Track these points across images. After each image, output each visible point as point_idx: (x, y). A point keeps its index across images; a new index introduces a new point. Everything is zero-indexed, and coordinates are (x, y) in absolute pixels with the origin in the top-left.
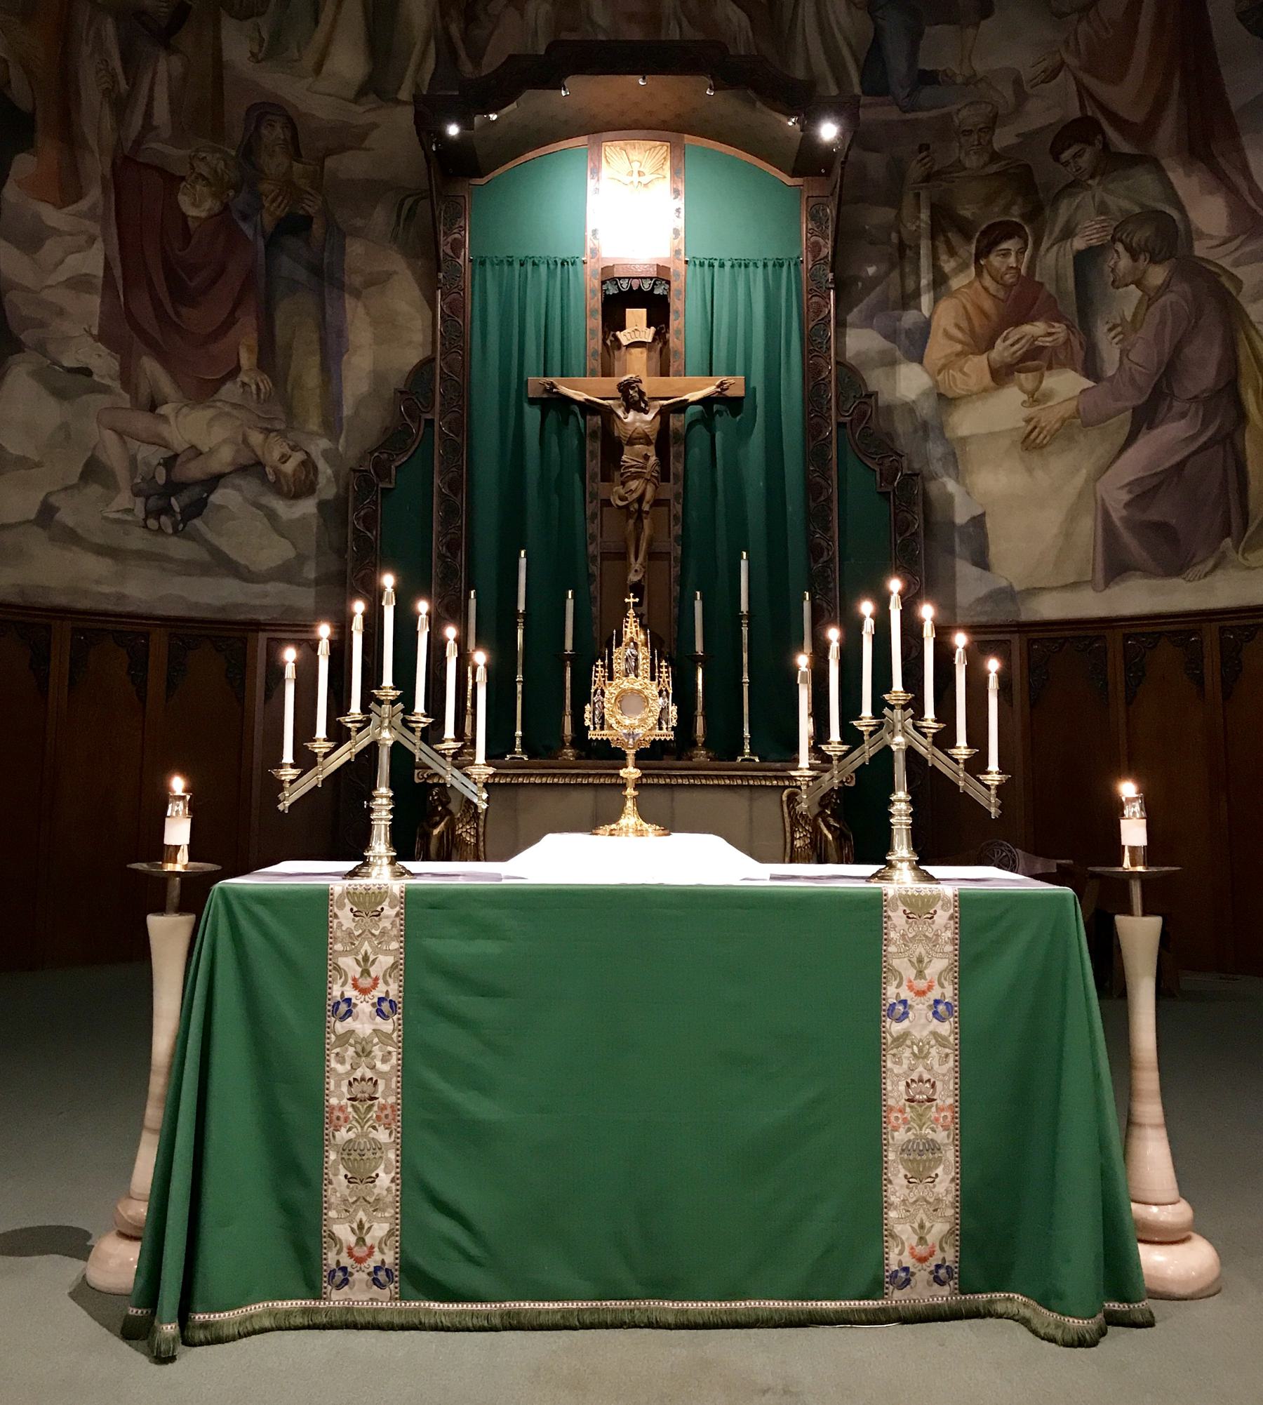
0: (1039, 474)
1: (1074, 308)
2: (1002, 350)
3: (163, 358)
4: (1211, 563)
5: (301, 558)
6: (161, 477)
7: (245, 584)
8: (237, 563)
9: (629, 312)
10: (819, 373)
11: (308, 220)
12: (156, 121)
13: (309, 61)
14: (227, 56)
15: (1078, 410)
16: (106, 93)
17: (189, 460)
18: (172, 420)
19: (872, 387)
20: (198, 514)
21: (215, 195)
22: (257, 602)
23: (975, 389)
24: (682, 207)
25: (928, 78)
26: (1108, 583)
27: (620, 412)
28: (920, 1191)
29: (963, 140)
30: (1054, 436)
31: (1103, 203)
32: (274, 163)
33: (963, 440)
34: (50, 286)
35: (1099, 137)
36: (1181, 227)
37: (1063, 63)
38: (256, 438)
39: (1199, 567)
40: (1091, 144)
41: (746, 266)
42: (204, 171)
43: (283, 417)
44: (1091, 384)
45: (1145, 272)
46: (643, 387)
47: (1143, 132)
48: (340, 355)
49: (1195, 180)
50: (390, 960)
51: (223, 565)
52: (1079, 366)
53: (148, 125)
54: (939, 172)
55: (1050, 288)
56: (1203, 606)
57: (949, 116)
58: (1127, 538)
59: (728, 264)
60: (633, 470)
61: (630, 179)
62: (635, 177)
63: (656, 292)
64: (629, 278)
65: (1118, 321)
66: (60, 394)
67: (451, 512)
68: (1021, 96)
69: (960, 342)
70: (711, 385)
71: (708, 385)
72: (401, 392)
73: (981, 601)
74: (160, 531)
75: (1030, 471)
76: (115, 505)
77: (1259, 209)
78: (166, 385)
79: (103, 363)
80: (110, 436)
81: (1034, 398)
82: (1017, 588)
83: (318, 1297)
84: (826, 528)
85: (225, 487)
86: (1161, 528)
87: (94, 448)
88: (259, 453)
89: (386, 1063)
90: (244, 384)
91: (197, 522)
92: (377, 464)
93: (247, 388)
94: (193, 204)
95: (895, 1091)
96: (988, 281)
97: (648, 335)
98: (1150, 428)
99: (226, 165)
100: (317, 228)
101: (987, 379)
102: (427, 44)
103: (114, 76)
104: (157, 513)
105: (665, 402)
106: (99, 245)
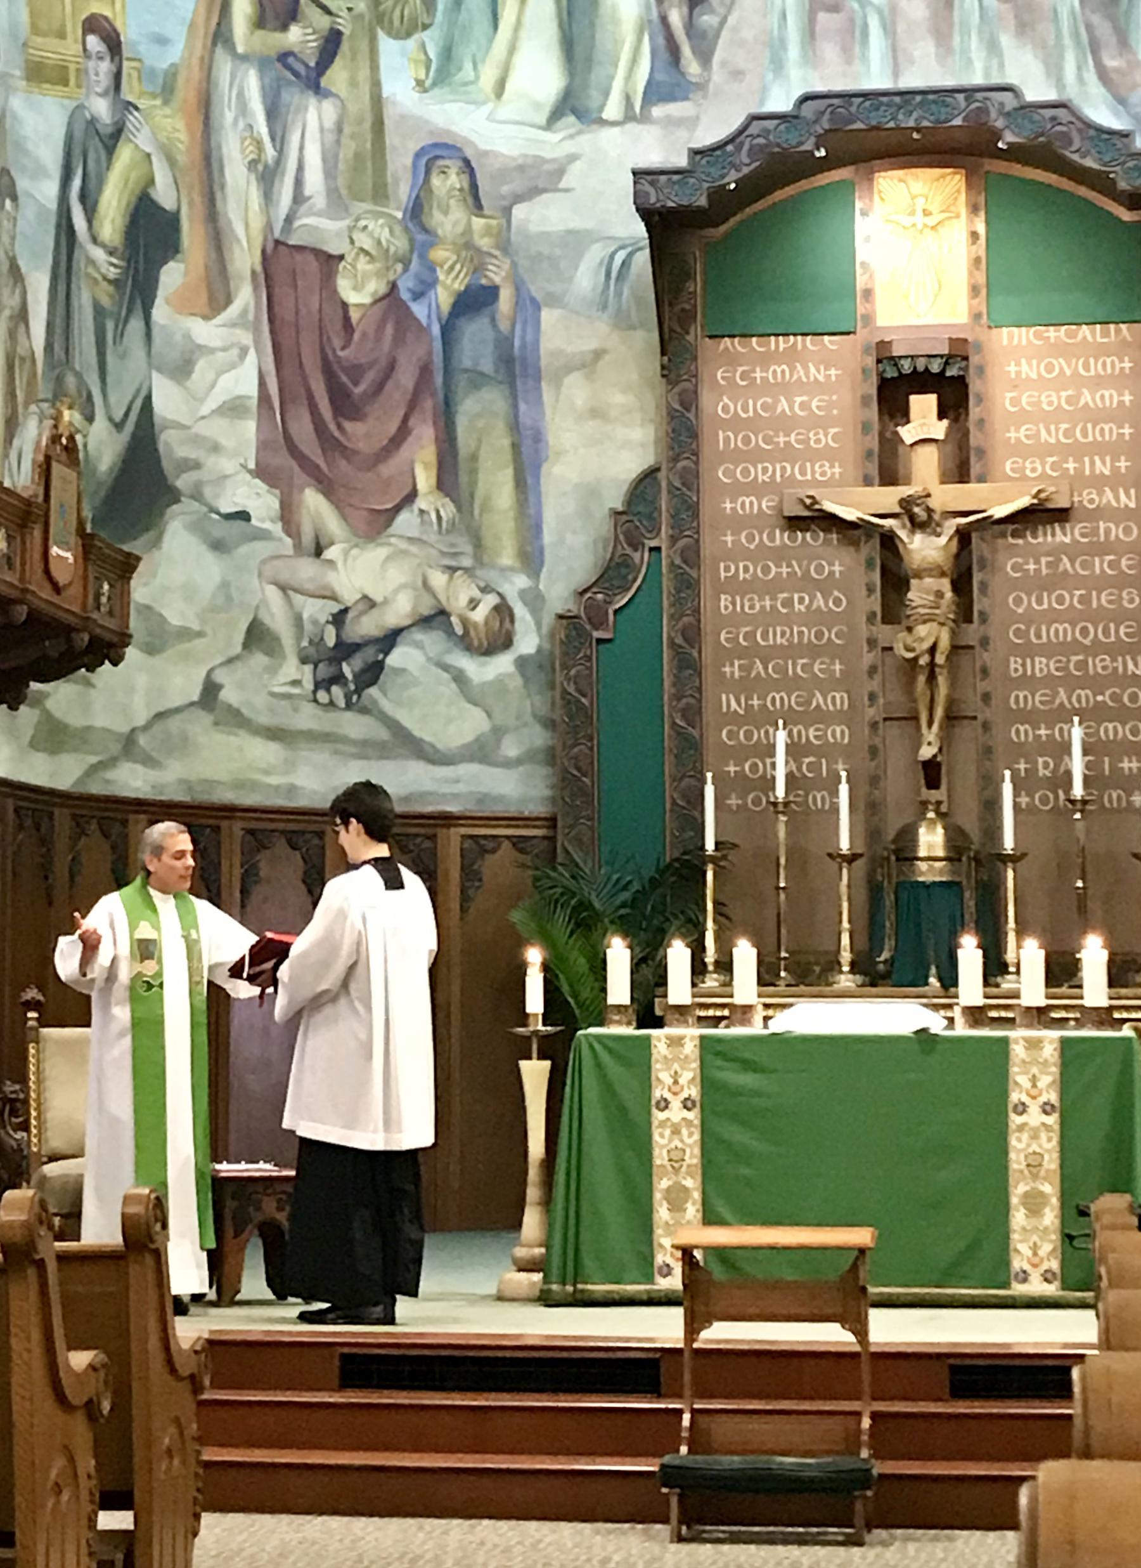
3: (327, 488)
5: (498, 732)
6: (331, 641)
7: (430, 767)
8: (421, 740)
11: (492, 292)
13: (488, 75)
14: (386, 91)
16: (252, 164)
18: (340, 565)
20: (373, 682)
21: (378, 274)
27: (903, 534)
28: (1034, 1221)
34: (203, 418)
38: (438, 579)
42: (368, 244)
43: (469, 549)
46: (933, 503)
48: (538, 467)
50: (690, 1075)
53: (299, 197)
60: (922, 611)
62: (919, 219)
63: (948, 374)
64: (912, 357)
66: (218, 546)
70: (1022, 495)
76: (282, 679)
78: (332, 523)
80: (272, 592)
83: (653, 1283)
87: (257, 607)
88: (442, 598)
89: (692, 1139)
90: (422, 512)
91: (373, 691)
92: (591, 606)
93: (426, 517)
94: (355, 288)
95: (1017, 1161)
97: (939, 429)
99: (391, 231)
102: (640, 40)
103: (259, 144)
106: (252, 358)
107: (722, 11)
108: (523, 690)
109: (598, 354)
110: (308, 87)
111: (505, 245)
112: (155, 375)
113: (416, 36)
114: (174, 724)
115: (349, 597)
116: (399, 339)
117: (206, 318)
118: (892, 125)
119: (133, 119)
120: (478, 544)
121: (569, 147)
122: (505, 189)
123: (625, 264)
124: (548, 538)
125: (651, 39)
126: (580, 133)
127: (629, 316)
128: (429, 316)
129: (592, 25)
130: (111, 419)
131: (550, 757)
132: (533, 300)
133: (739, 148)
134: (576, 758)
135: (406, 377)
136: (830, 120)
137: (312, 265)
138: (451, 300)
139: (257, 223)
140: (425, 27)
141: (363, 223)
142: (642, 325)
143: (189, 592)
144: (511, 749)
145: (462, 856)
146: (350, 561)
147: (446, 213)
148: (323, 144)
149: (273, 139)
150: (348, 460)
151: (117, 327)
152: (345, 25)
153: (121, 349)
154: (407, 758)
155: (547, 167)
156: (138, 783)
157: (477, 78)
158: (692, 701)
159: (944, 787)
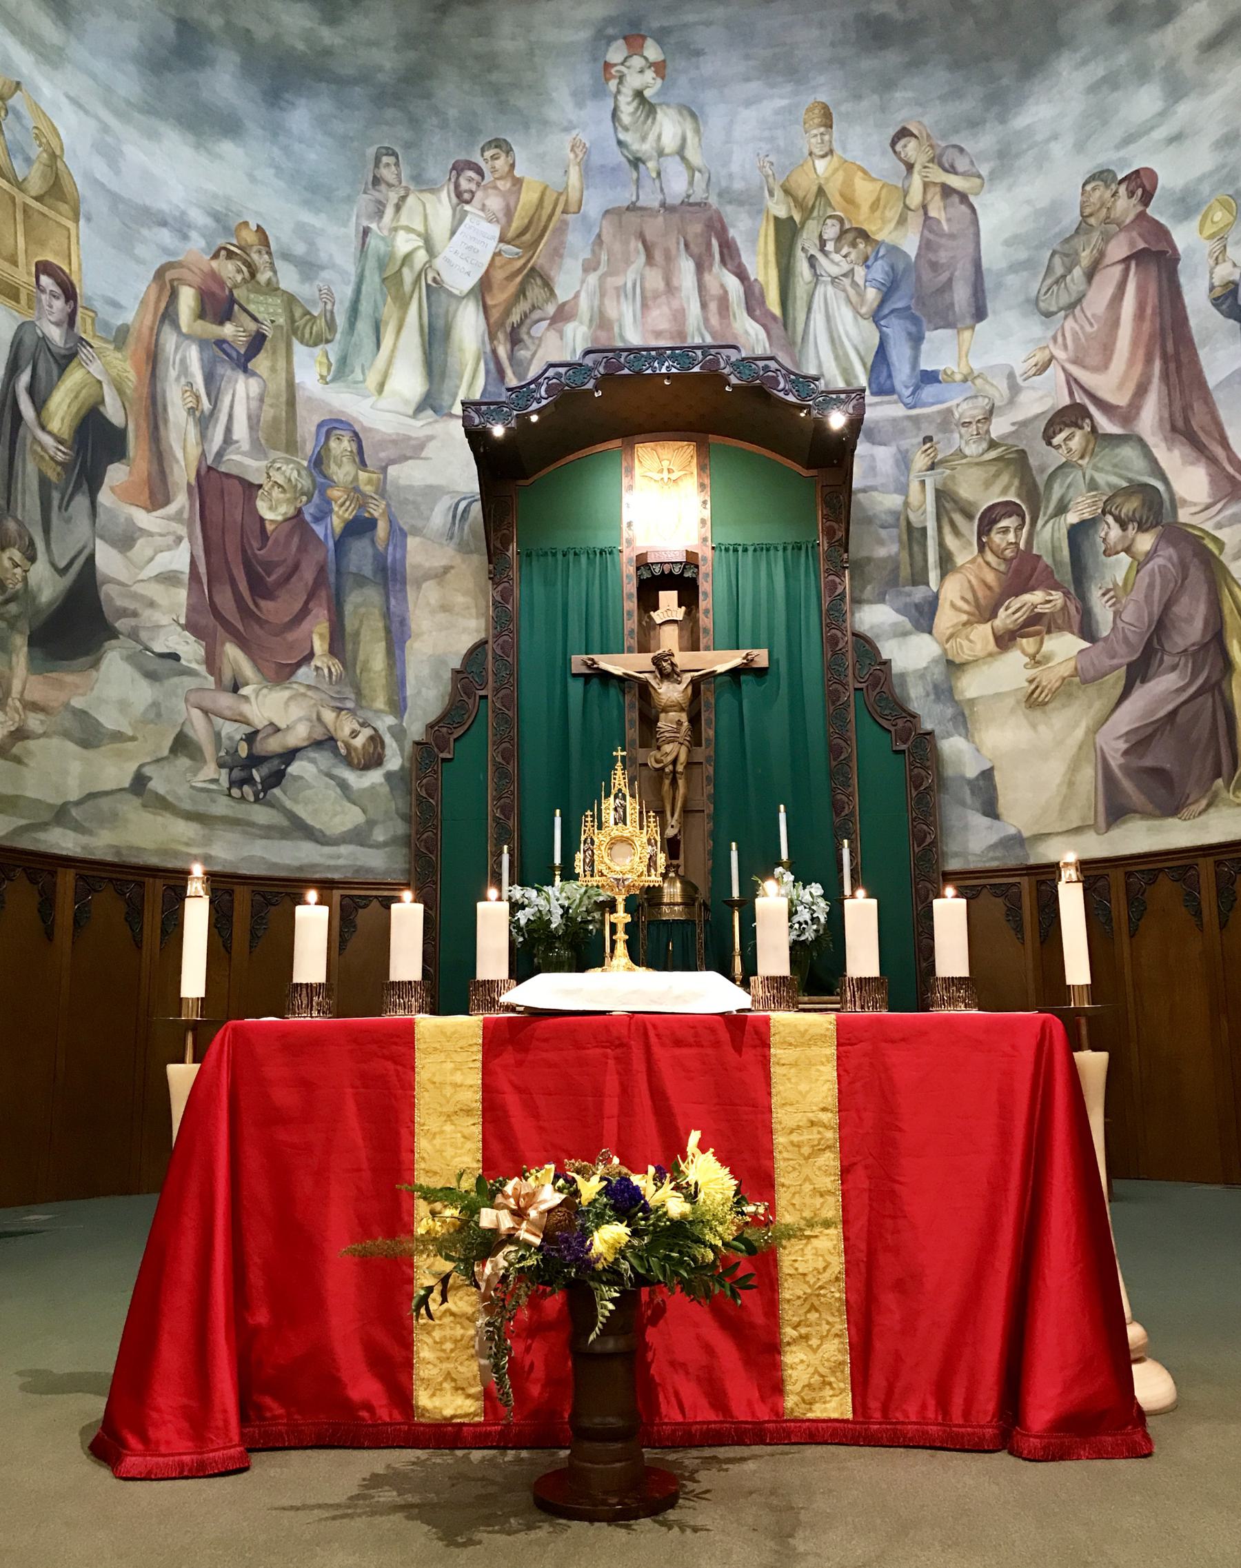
0: (1042, 728)
1: (1069, 577)
2: (1005, 619)
3: (243, 643)
4: (1204, 803)
5: (371, 823)
6: (243, 751)
7: (319, 847)
8: (313, 827)
9: (663, 595)
10: (837, 644)
11: (371, 524)
12: (236, 436)
13: (373, 379)
15: (1076, 669)
16: (191, 411)
17: (268, 736)
18: (253, 699)
19: (885, 656)
21: (288, 501)
22: (332, 862)
23: (981, 654)
24: (708, 499)
25: (930, 377)
26: (1109, 826)
29: (963, 430)
30: (1055, 693)
31: (1092, 479)
32: (342, 471)
33: (972, 702)
34: (142, 581)
35: (1088, 421)
36: (1165, 496)
37: (1052, 358)
38: (329, 716)
39: (1192, 808)
40: (1081, 428)
41: (768, 550)
43: (352, 696)
44: (1086, 645)
45: (1133, 540)
46: (676, 660)
47: (1127, 415)
49: (1176, 453)
51: (301, 829)
52: (1076, 629)
53: (228, 440)
54: (942, 462)
55: (1047, 560)
56: (1199, 843)
57: (949, 411)
58: (1127, 784)
59: (751, 549)
60: (667, 735)
61: (660, 476)
62: (665, 475)
65: (1111, 586)
66: (151, 676)
67: (501, 773)
68: (1014, 389)
69: (965, 612)
71: (735, 657)
72: (458, 672)
73: (993, 847)
74: (243, 798)
75: (1034, 726)
77: (1237, 475)
78: (247, 669)
79: (190, 650)
80: (196, 714)
81: (1036, 660)
82: (1026, 834)
84: (846, 783)
85: (302, 759)
86: (1157, 773)
87: (183, 724)
88: (332, 730)
90: (317, 668)
94: (271, 508)
96: (990, 557)
97: (679, 614)
98: (1143, 681)
100: (382, 529)
101: (992, 646)
103: (198, 398)
104: (240, 783)
105: (696, 674)
106: (185, 544)
107: (533, 348)
108: (390, 797)
109: (447, 570)
110: (238, 366)
111: (382, 491)
112: (98, 542)
113: (321, 346)
114: (105, 803)
115: (259, 720)
116: (302, 549)
117: (149, 511)
118: (649, 371)
119: (84, 352)
120: (359, 694)
121: (428, 431)
122: (382, 455)
123: (466, 510)
124: (410, 691)
125: (486, 364)
126: (436, 421)
127: (468, 544)
128: (326, 535)
129: (446, 353)
130: (53, 565)
131: (407, 841)
132: (401, 529)
133: (541, 385)
134: (426, 841)
135: (308, 574)
136: (605, 367)
137: (239, 488)
138: (342, 525)
139: (194, 451)
140: (328, 341)
141: (278, 465)
142: (477, 551)
143: (123, 705)
144: (379, 835)
145: (342, 910)
146: (260, 697)
147: (340, 466)
148: (248, 409)
149: (208, 395)
150: (261, 627)
151: (62, 499)
152: (268, 331)
153: (66, 515)
154: (301, 839)
155: (413, 442)
156: (70, 845)
157: (364, 381)
158: (508, 801)
159: (682, 856)
